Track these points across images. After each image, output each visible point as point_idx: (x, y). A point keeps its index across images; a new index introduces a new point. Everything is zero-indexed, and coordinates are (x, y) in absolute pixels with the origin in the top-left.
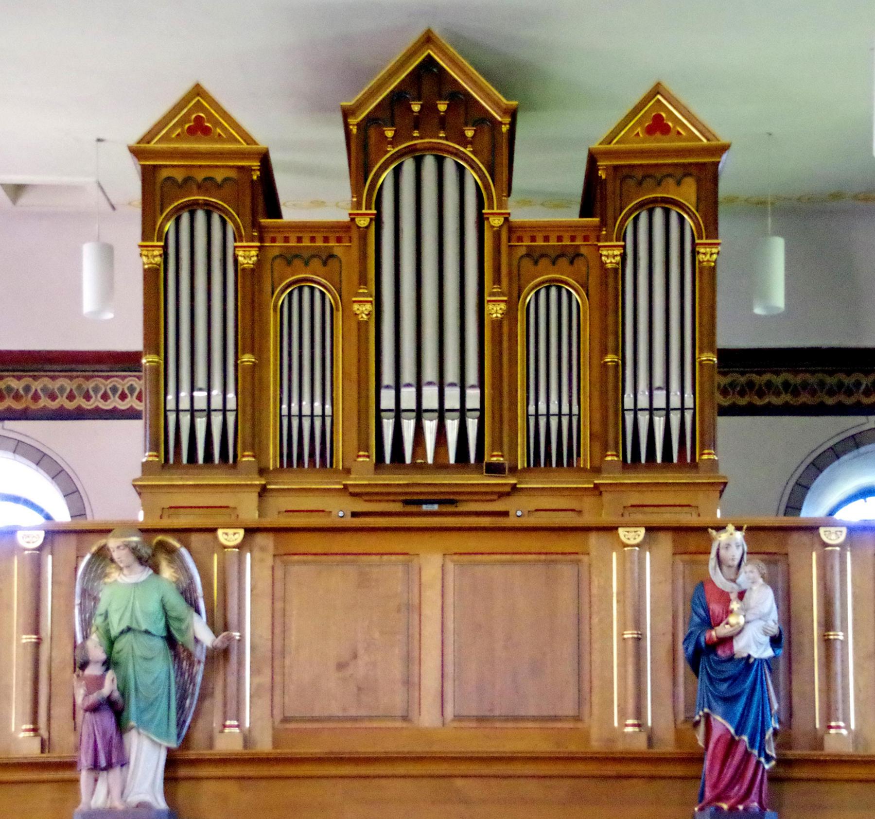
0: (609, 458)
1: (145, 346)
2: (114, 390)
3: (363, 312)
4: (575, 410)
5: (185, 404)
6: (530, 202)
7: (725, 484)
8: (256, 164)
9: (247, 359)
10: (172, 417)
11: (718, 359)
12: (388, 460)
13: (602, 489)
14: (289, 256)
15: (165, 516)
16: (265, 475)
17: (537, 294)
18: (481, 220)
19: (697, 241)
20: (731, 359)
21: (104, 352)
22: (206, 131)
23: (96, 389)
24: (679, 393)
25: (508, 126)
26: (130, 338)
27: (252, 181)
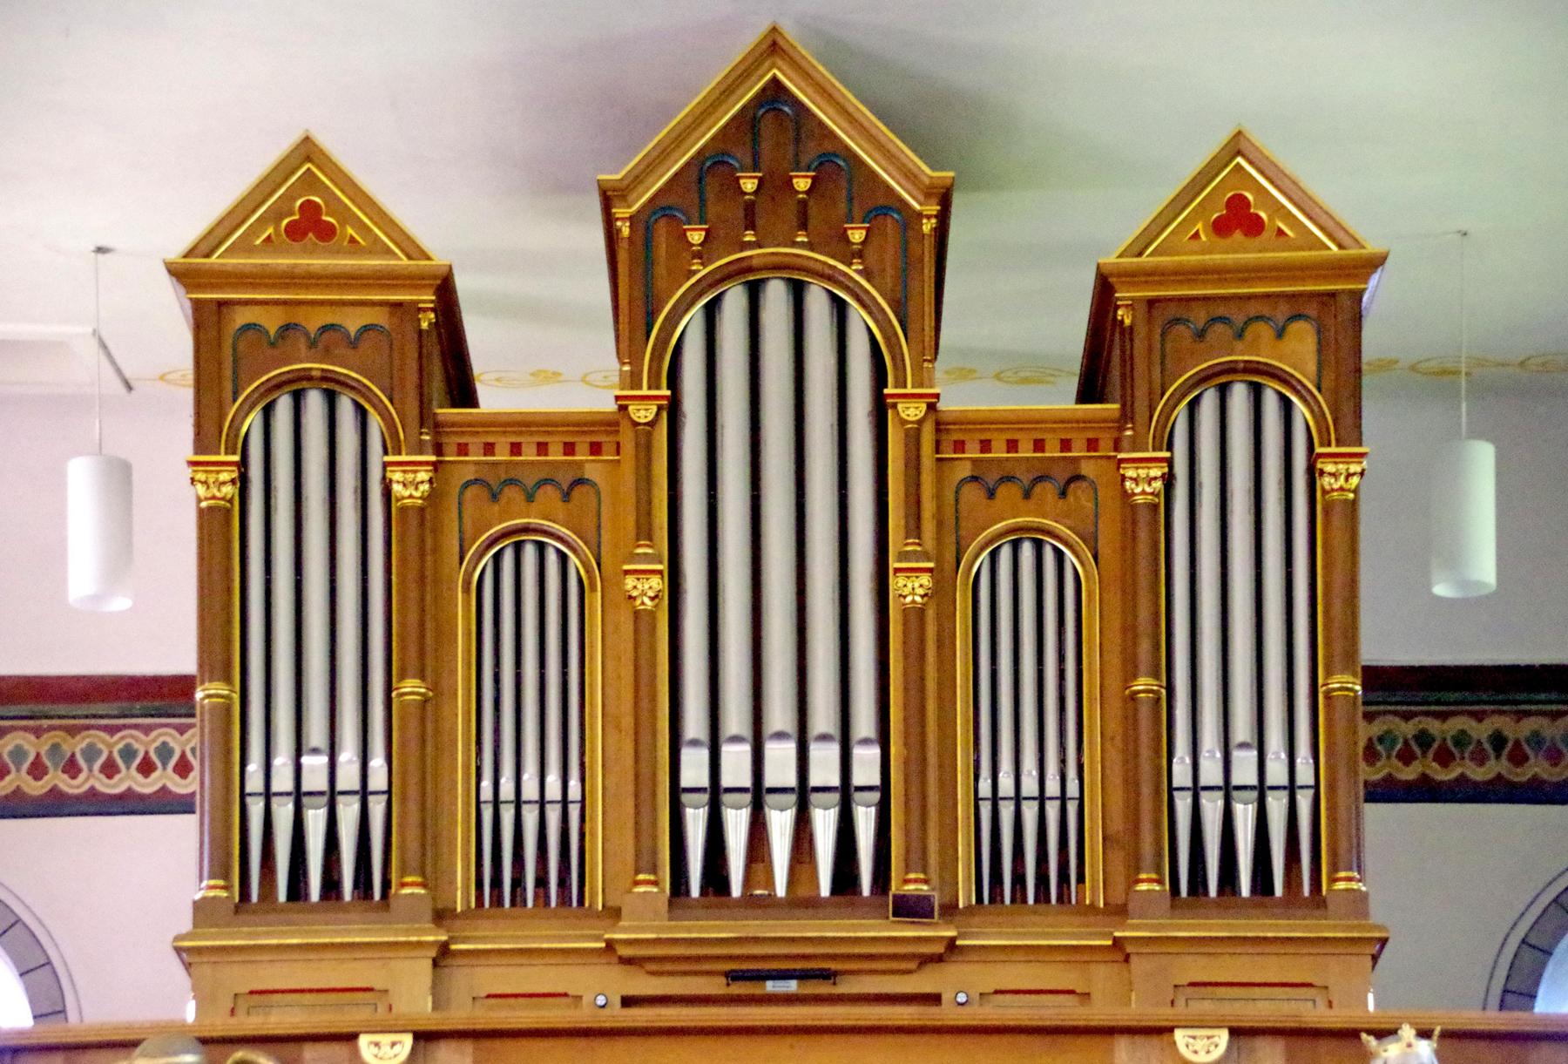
0: (1143, 887)
1: (201, 666)
2: (128, 754)
3: (644, 594)
4: (1073, 789)
5: (283, 780)
6: (971, 371)
7: (1383, 942)
8: (427, 298)
9: (411, 687)
10: (256, 809)
11: (1364, 689)
12: (695, 891)
13: (1129, 949)
14: (494, 484)
15: (241, 1011)
16: (447, 923)
17: (994, 556)
18: (880, 409)
19: (1319, 450)
20: (1387, 684)
21: (35, 677)
22: (326, 232)
23: (91, 753)
24: (1283, 756)
25: (934, 221)
26: (172, 649)
27: (420, 332)
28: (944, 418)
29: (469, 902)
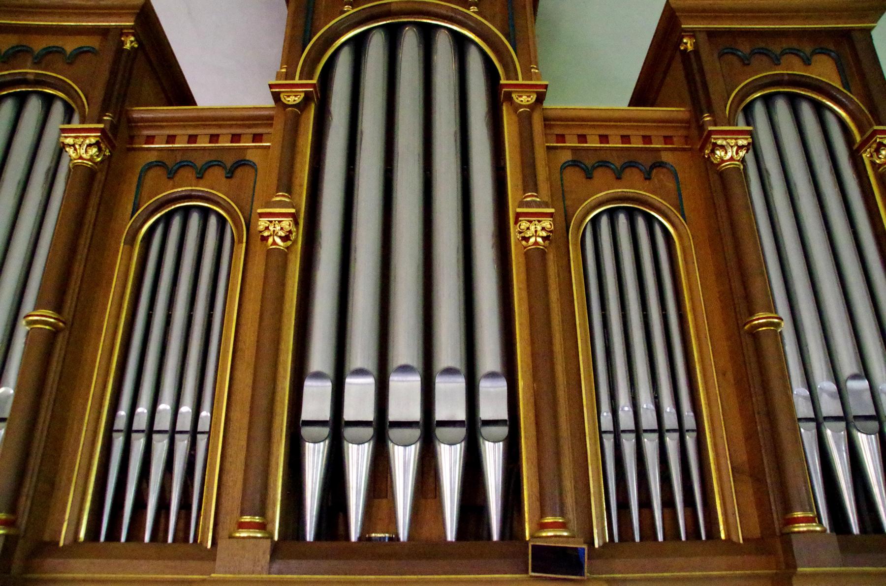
4: (689, 421)
28: (551, 114)
29: (77, 532)
